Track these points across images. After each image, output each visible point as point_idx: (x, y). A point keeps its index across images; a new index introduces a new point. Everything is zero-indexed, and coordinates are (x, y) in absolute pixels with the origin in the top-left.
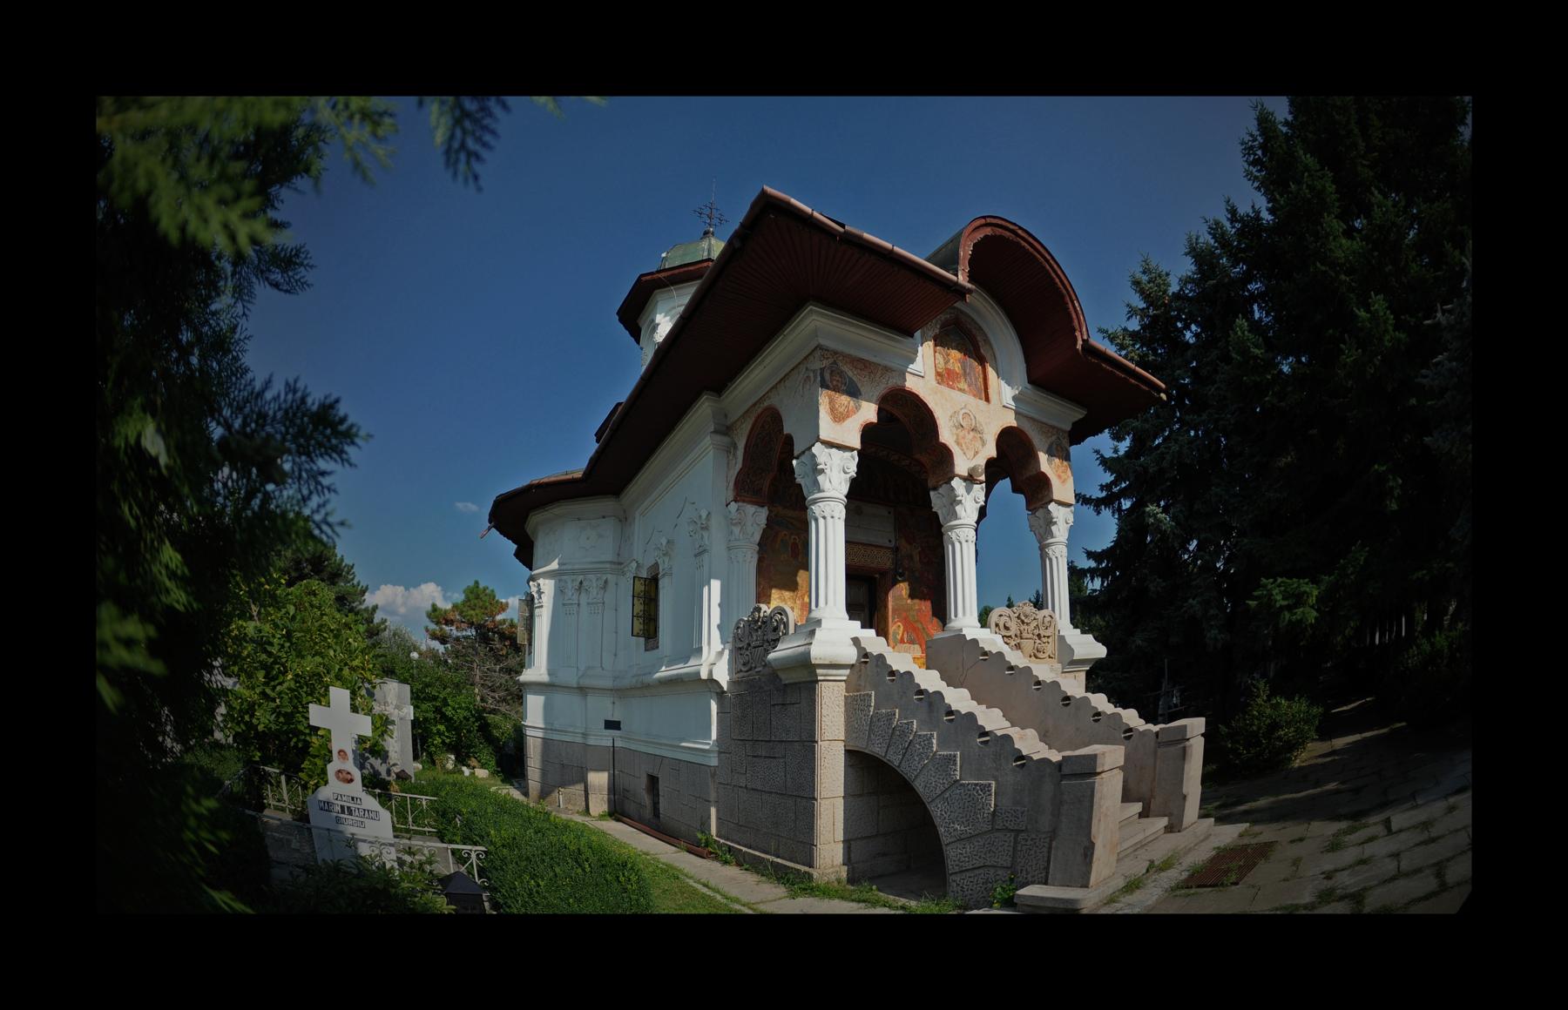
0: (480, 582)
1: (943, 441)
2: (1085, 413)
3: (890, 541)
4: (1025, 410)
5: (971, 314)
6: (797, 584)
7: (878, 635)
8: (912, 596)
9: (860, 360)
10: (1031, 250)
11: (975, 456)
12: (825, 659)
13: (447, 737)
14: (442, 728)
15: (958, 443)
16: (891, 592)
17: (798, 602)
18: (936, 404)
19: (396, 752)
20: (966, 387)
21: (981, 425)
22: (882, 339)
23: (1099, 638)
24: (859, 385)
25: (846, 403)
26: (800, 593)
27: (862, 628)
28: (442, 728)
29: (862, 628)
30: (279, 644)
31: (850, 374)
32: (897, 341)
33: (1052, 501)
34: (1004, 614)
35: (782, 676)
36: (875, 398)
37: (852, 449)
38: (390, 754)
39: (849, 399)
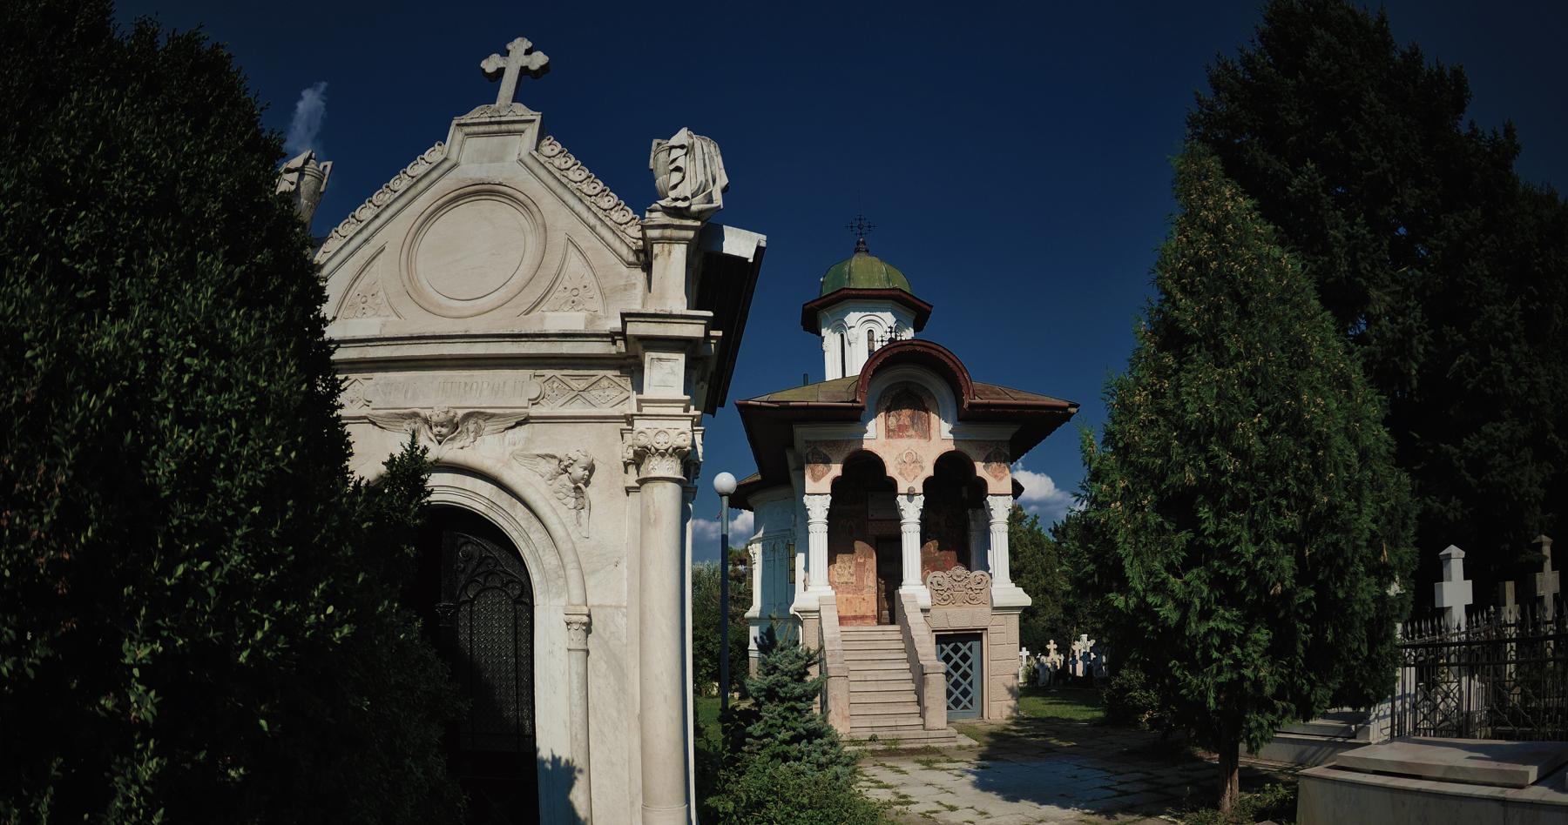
8: (940, 549)
10: (925, 350)
13: (710, 667)
14: (705, 660)
15: (901, 474)
20: (913, 433)
21: (921, 457)
23: (473, 546)
24: (830, 456)
27: (1466, 606)
28: (705, 660)
29: (1466, 606)
31: (824, 451)
33: (988, 495)
35: (435, 480)
37: (826, 494)
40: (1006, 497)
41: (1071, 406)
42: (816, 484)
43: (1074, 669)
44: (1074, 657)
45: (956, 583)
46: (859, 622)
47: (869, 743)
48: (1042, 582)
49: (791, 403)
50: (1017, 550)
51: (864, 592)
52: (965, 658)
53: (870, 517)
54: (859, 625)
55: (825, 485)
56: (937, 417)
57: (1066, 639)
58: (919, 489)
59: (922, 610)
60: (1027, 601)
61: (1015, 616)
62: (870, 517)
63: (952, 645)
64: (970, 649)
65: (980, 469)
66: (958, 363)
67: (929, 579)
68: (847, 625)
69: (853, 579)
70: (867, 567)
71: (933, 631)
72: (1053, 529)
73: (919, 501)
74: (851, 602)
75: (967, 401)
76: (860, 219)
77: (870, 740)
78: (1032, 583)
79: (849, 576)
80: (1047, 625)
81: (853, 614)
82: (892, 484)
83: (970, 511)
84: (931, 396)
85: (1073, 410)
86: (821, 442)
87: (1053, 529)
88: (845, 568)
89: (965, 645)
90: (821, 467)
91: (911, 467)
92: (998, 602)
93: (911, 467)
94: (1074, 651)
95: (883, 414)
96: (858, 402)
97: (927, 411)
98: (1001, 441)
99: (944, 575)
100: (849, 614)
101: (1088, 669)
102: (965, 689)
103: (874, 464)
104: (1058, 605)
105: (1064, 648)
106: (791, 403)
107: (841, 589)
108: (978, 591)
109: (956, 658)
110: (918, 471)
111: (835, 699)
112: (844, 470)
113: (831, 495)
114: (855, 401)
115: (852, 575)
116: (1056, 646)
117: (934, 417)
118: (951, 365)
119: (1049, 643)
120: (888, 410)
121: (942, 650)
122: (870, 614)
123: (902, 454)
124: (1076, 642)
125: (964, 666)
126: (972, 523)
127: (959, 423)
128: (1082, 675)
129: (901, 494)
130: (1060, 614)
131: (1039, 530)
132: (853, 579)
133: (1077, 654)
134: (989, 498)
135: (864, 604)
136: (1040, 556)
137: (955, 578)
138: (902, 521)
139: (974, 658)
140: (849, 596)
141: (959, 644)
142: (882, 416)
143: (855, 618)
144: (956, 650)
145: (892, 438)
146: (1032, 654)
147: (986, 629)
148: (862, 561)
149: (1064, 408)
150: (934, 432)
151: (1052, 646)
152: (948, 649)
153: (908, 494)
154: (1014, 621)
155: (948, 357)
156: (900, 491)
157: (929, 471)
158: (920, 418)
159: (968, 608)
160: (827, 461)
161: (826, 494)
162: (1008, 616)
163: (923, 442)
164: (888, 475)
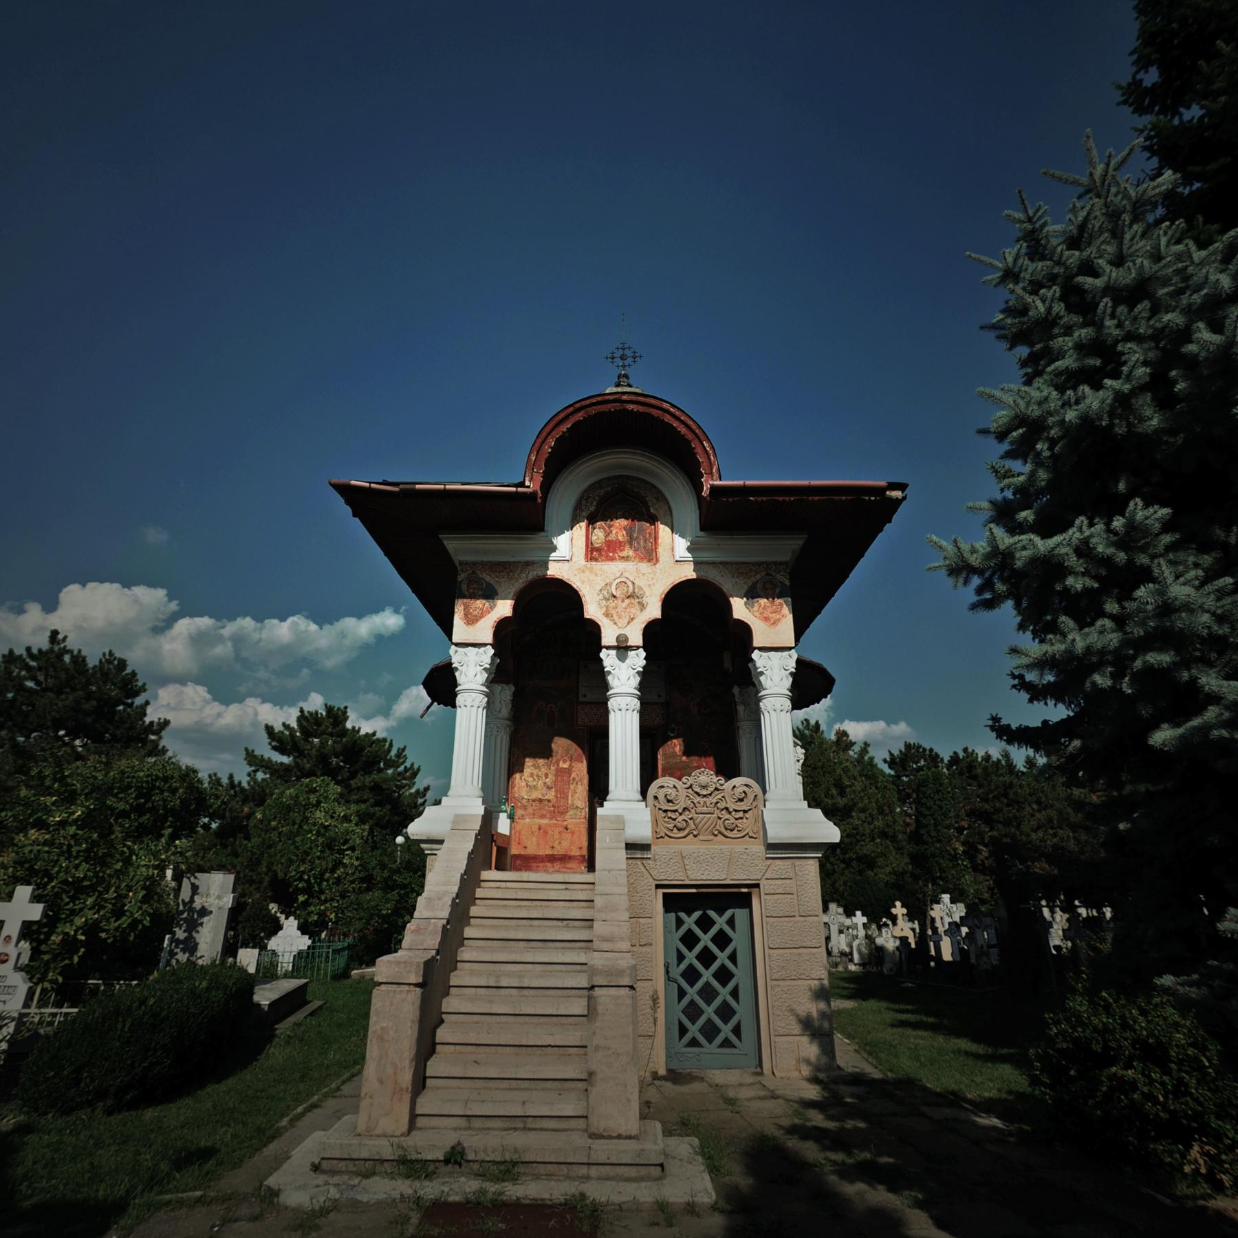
0: (234, 775)
1: (588, 617)
2: (807, 536)
3: (659, 696)
4: (706, 556)
5: (638, 476)
6: (551, 751)
7: (810, 806)
9: (499, 564)
10: (641, 409)
11: (629, 623)
12: (421, 835)
15: (607, 615)
16: (661, 750)
17: (552, 768)
18: (583, 582)
19: (206, 943)
20: (631, 553)
22: (512, 542)
24: (496, 587)
25: (481, 606)
26: (554, 759)
30: (829, 878)
31: (488, 579)
32: (528, 539)
34: (665, 785)
36: (511, 595)
37: (485, 645)
38: (199, 947)
39: (484, 601)
40: (786, 653)
41: (893, 486)
42: (471, 628)
43: (938, 949)
44: (935, 930)
45: (698, 799)
46: (557, 865)
47: (444, 1169)
48: (879, 823)
49: (418, 486)
50: (843, 783)
51: (567, 816)
52: (722, 940)
53: (581, 699)
54: (558, 871)
55: (484, 631)
56: (668, 530)
57: (918, 899)
58: (636, 638)
59: (630, 847)
60: (831, 833)
61: (811, 862)
62: (581, 699)
63: (697, 914)
64: (731, 922)
65: (740, 608)
66: (694, 427)
67: (653, 789)
68: (537, 871)
69: (551, 795)
70: (573, 775)
71: (658, 887)
72: (888, 759)
73: (638, 659)
74: (546, 832)
75: (708, 483)
76: (623, 358)
77: (447, 1161)
78: (866, 825)
79: (545, 790)
80: (892, 879)
81: (549, 852)
82: (594, 630)
83: (736, 690)
84: (661, 498)
85: (897, 494)
86: (483, 564)
87: (888, 759)
88: (538, 776)
89: (721, 914)
90: (479, 603)
91: (624, 605)
92: (777, 833)
93: (624, 605)
94: (933, 920)
95: (583, 524)
96: (529, 487)
97: (653, 520)
98: (775, 563)
99: (679, 784)
100: (541, 853)
101: (957, 949)
102: (725, 1004)
103: (567, 596)
104: (902, 854)
105: (918, 912)
106: (418, 486)
107: (530, 810)
108: (741, 815)
109: (706, 940)
110: (635, 610)
111: (381, 1039)
112: (515, 608)
113: (493, 646)
114: (522, 484)
115: (549, 788)
116: (905, 911)
117: (663, 530)
118: (683, 430)
119: (895, 907)
120: (592, 520)
121: (679, 922)
122: (575, 852)
123: (611, 584)
124: (935, 906)
125: (722, 957)
126: (740, 708)
127: (702, 534)
128: (951, 959)
129: (608, 648)
130: (907, 864)
131: (872, 759)
132: (551, 795)
133: (938, 924)
134: (755, 655)
135: (567, 836)
136: (873, 790)
137: (698, 790)
138: (610, 692)
139: (738, 940)
140: (544, 822)
141: (712, 914)
142: (580, 529)
143: (552, 859)
144: (705, 924)
145: (596, 560)
146: (871, 920)
147: (757, 886)
148: (566, 766)
149: (879, 491)
150: (663, 551)
151: (899, 910)
152: (690, 921)
153: (617, 648)
154: (810, 869)
155: (678, 419)
156: (605, 642)
157: (654, 611)
158: (641, 531)
159: (721, 846)
160: (490, 594)
161: (485, 645)
162: (798, 862)
163: (644, 567)
164: (587, 616)
